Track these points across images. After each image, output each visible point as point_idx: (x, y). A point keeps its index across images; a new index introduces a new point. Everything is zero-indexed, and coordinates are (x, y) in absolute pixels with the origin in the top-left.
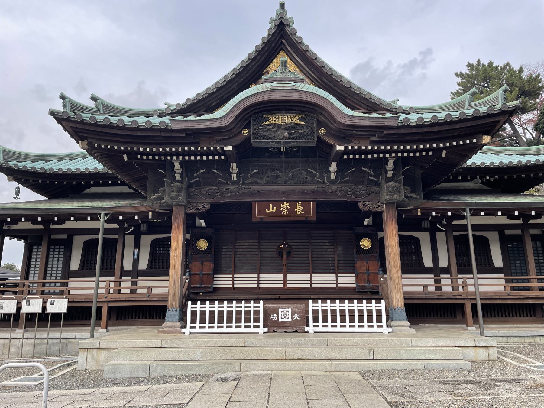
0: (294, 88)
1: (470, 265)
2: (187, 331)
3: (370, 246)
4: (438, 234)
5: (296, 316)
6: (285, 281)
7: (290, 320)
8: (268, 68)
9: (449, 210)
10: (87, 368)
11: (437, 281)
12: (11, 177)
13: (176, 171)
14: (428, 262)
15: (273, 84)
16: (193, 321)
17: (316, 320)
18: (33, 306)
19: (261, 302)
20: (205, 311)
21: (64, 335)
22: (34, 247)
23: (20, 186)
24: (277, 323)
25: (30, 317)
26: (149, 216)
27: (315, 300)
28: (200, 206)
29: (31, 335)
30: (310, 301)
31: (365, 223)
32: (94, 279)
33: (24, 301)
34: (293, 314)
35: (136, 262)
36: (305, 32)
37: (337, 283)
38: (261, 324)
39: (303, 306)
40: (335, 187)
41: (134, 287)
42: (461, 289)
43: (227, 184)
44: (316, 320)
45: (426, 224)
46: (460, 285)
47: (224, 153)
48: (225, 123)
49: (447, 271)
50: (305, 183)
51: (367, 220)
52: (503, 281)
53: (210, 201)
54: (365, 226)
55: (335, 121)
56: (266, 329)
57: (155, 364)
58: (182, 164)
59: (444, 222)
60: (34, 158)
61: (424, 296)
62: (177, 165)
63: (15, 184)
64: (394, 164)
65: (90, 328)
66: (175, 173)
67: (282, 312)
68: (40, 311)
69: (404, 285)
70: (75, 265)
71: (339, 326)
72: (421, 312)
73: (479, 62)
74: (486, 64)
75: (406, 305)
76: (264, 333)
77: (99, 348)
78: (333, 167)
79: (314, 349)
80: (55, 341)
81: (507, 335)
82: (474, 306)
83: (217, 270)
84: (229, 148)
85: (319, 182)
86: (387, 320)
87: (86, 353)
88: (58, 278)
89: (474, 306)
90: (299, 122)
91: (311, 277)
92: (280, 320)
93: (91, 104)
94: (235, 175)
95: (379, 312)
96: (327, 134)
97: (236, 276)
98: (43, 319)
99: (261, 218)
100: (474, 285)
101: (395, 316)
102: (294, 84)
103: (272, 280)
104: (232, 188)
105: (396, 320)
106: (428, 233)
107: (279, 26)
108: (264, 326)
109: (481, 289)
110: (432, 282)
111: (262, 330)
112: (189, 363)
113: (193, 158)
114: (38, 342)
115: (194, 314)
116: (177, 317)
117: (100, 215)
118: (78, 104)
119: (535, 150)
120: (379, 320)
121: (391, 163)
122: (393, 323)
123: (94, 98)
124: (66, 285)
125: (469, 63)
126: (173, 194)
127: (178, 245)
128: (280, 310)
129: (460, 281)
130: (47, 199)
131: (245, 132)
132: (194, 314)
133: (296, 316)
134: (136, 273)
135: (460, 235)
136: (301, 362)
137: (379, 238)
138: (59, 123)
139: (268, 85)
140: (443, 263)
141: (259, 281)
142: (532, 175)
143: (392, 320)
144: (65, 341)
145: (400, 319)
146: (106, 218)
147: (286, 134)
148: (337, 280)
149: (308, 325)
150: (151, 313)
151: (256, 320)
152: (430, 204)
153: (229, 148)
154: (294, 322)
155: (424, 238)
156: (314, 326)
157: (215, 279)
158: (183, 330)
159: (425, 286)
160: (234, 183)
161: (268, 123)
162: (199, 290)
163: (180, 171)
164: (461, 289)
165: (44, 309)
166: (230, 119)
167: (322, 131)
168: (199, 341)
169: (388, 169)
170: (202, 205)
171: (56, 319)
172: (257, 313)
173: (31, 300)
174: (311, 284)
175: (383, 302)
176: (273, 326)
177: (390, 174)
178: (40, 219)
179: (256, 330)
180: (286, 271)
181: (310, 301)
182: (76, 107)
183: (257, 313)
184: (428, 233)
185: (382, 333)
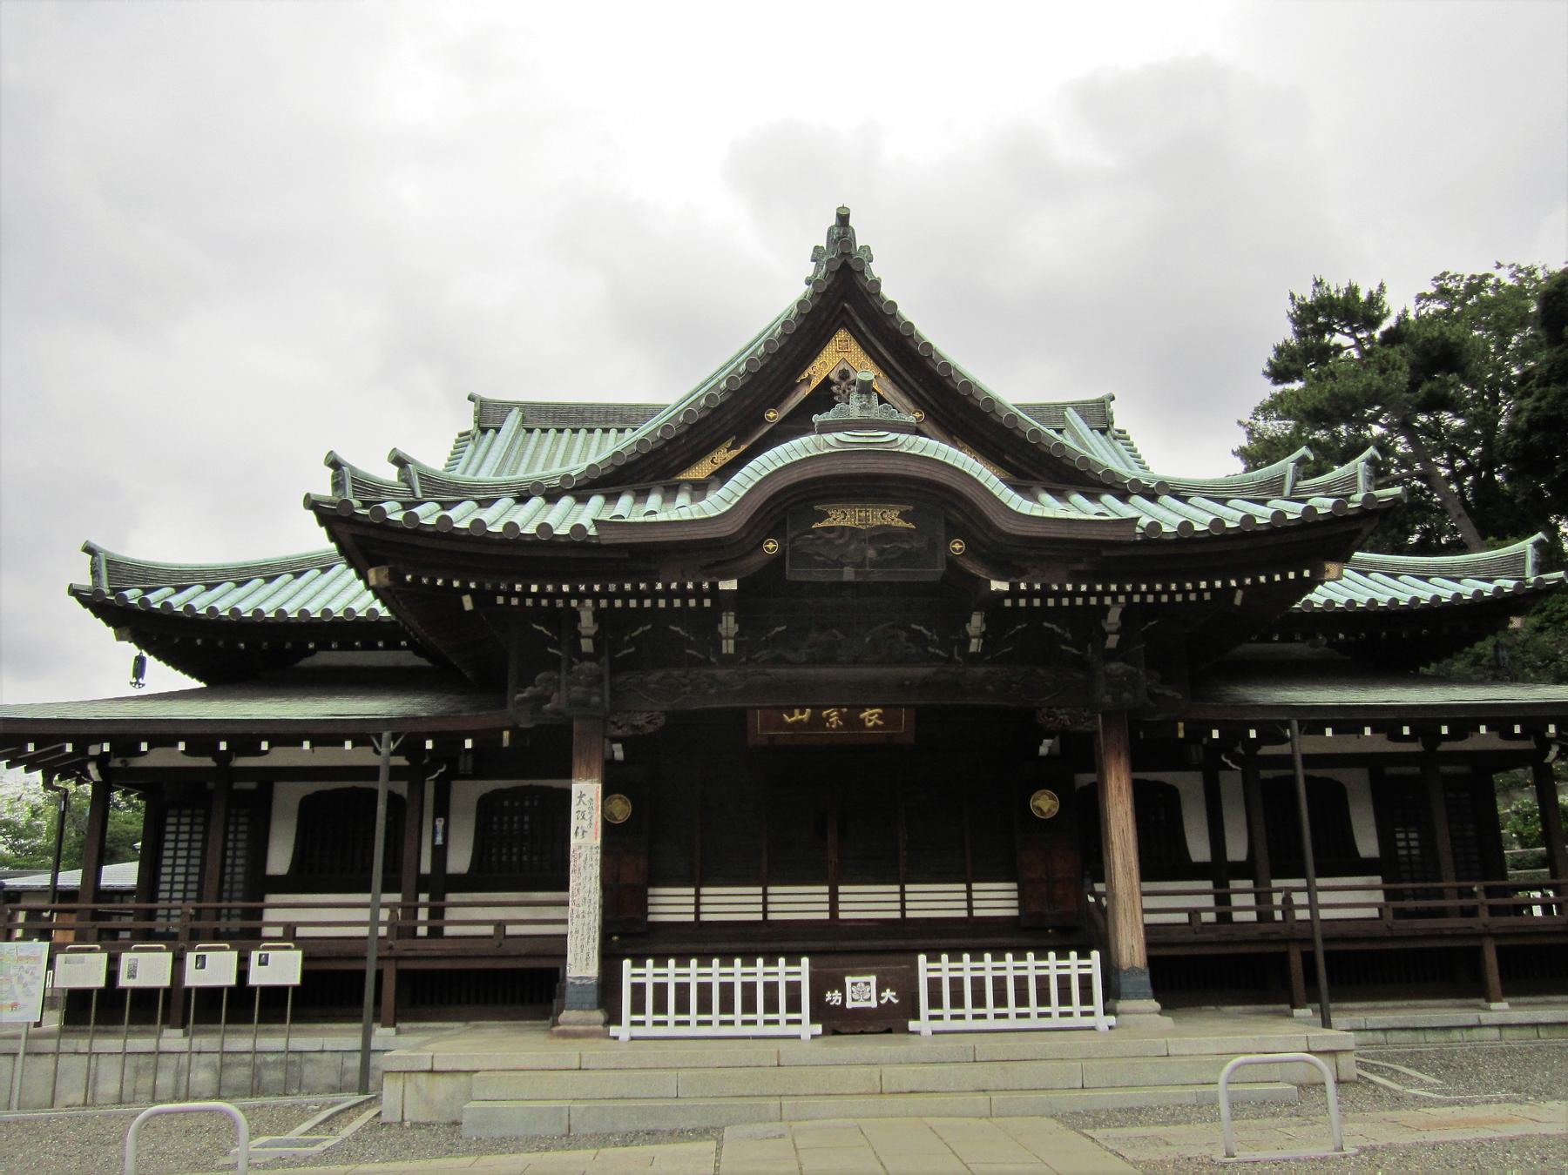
0: (889, 448)
1: (1300, 855)
2: (623, 1031)
3: (1055, 810)
4: (1222, 774)
7: (873, 1004)
8: (809, 371)
9: (1252, 725)
10: (406, 1117)
11: (1223, 899)
12: (126, 632)
13: (583, 632)
14: (1199, 850)
15: (841, 436)
16: (638, 1007)
17: (935, 1001)
18: (215, 968)
19: (805, 961)
20: (666, 985)
21: (299, 1043)
22: (171, 812)
23: (145, 654)
25: (209, 996)
26: (501, 739)
27: (933, 956)
28: (640, 720)
29: (206, 1042)
30: (922, 958)
31: (1043, 750)
33: (191, 957)
34: (880, 988)
36: (901, 284)
40: (980, 671)
41: (436, 923)
42: (1278, 915)
43: (707, 663)
44: (935, 1001)
45: (1196, 753)
46: (1278, 908)
47: (714, 591)
48: (728, 529)
49: (1240, 871)
50: (904, 660)
51: (1047, 742)
53: (666, 707)
54: (1044, 757)
55: (989, 525)
56: (818, 1029)
57: (577, 1105)
58: (598, 615)
59: (1240, 750)
60: (181, 579)
61: (1192, 937)
62: (587, 622)
63: (131, 650)
64: (1122, 616)
65: (360, 1025)
67: (854, 984)
68: (233, 982)
69: (1145, 911)
70: (279, 861)
71: (969, 1017)
75: (1152, 961)
76: (813, 1037)
77: (431, 1071)
78: (976, 623)
79: (945, 1067)
80: (270, 1058)
81: (1385, 1026)
82: (1309, 960)
84: (730, 585)
85: (937, 658)
86: (1106, 998)
87: (400, 1083)
89: (1309, 960)
90: (902, 524)
91: (902, 892)
92: (849, 1005)
93: (390, 474)
94: (731, 642)
95: (1086, 981)
96: (971, 550)
97: (704, 890)
98: (241, 1004)
99: (772, 738)
100: (1307, 889)
101: (1126, 987)
102: (892, 436)
103: (800, 903)
104: (721, 673)
105: (1128, 997)
106: (1199, 774)
108: (813, 1020)
110: (1209, 901)
111: (809, 1029)
112: (660, 1103)
113: (633, 603)
114: (228, 1058)
115: (638, 990)
118: (367, 477)
120: (1087, 998)
122: (1122, 1005)
123: (400, 461)
124: (257, 914)
126: (577, 692)
128: (848, 980)
129: (1277, 899)
130: (203, 685)
131: (771, 546)
132: (638, 990)
138: (321, 524)
139: (830, 438)
140: (1237, 850)
143: (1118, 997)
144: (296, 1058)
145: (1137, 996)
146: (392, 747)
147: (871, 553)
149: (917, 1017)
150: (520, 987)
153: (730, 585)
154: (884, 1010)
155: (1189, 784)
156: (932, 1018)
158: (613, 1030)
159: (1194, 913)
160: (728, 661)
161: (825, 524)
163: (592, 632)
164: (1278, 915)
168: (650, 1052)
169: (1107, 628)
170: (644, 715)
171: (272, 1005)
172: (794, 988)
173: (208, 954)
174: (903, 910)
175: (1095, 954)
176: (836, 1021)
177: (1112, 641)
179: (793, 1030)
180: (834, 877)
181: (922, 958)
182: (370, 489)
183: (794, 988)
184: (1199, 774)
185: (1093, 1028)
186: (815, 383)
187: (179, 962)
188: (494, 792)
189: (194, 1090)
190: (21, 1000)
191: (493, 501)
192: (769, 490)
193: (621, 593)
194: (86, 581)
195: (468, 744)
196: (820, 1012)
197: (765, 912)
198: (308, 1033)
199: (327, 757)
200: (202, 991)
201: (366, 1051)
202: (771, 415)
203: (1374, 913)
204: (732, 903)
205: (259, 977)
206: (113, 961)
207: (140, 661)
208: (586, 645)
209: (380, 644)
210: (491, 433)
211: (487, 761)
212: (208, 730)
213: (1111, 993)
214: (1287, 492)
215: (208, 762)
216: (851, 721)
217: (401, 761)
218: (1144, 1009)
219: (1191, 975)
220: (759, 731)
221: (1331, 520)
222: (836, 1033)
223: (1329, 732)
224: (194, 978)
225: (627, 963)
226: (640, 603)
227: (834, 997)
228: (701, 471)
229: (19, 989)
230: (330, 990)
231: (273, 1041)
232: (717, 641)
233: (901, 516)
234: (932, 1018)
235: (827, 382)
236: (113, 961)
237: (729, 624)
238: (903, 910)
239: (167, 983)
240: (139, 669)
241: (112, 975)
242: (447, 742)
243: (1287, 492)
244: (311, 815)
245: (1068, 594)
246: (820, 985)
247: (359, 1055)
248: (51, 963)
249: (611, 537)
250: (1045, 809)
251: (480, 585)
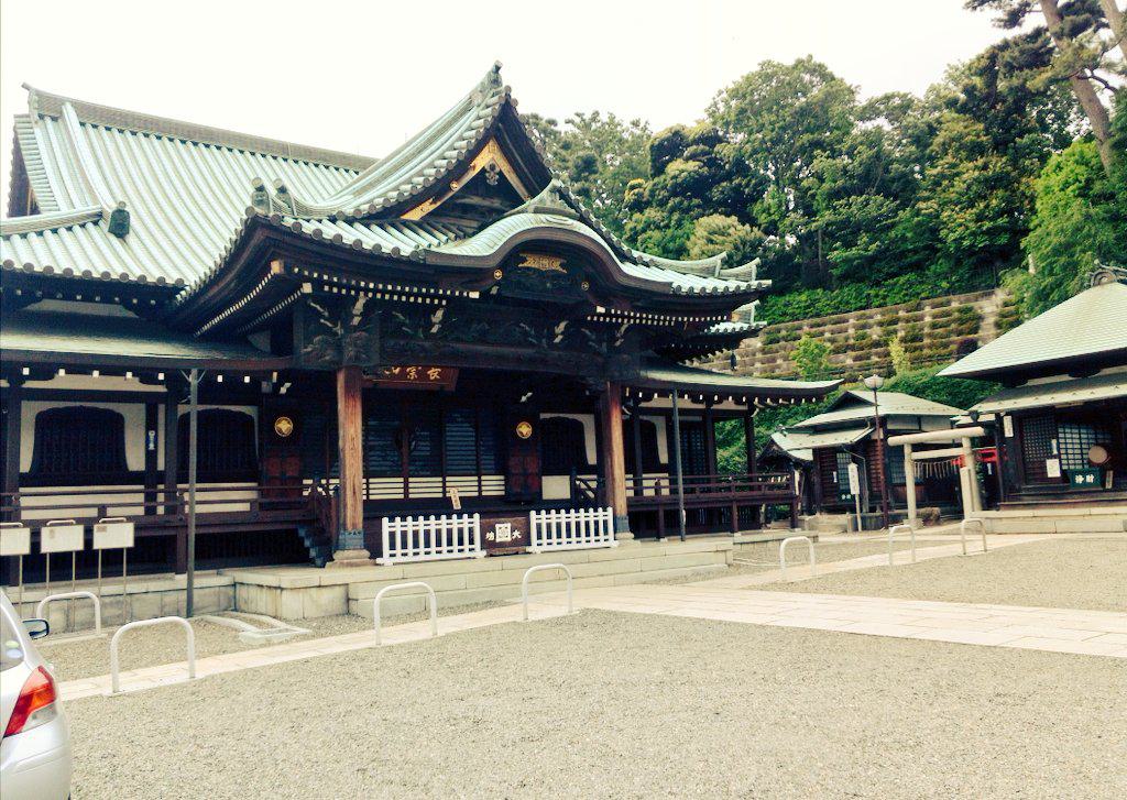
2: (385, 559)
6: (406, 488)
7: (509, 539)
15: (548, 217)
34: (513, 531)
35: (151, 457)
56: (485, 553)
75: (629, 514)
77: (320, 586)
86: (615, 532)
88: (652, 483)
98: (88, 563)
121: (359, 305)
127: (356, 431)
128: (497, 526)
133: (516, 534)
135: (67, 408)
137: (179, 414)
154: (515, 542)
157: (503, 488)
161: (525, 265)
169: (354, 312)
176: (492, 548)
177: (356, 320)
178: (161, 377)
186: (478, 170)
188: (53, 409)
189: (136, 611)
193: (340, 286)
196: (486, 544)
198: (111, 583)
200: (106, 552)
201: (190, 589)
202: (454, 185)
203: (245, 507)
209: (79, 297)
212: (14, 357)
214: (717, 274)
216: (422, 375)
219: (647, 522)
222: (491, 556)
226: (331, 289)
227: (490, 536)
231: (112, 586)
233: (561, 265)
234: (391, 555)
235: (483, 170)
243: (717, 274)
245: (388, 292)
247: (185, 592)
250: (525, 433)
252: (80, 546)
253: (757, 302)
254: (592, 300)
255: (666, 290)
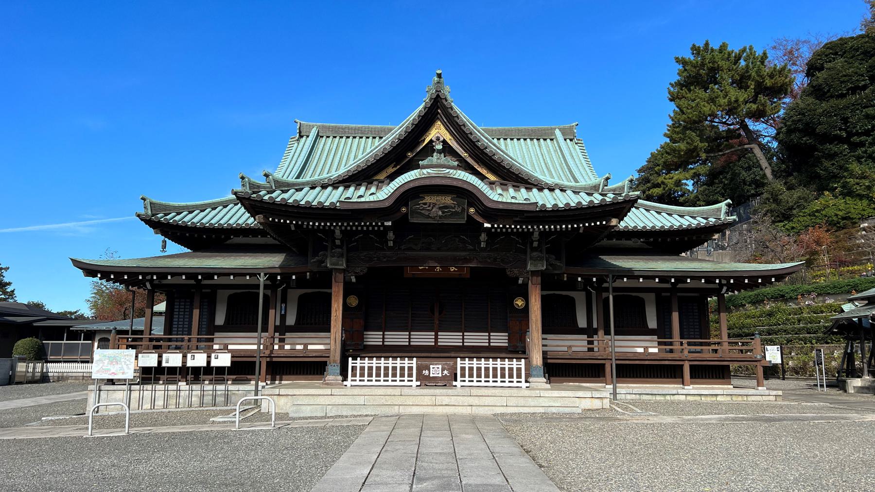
2: (348, 383)
5: (446, 372)
6: (436, 339)
7: (440, 375)
14: (582, 323)
15: (429, 170)
16: (354, 375)
17: (463, 375)
18: (198, 360)
24: (428, 378)
27: (463, 358)
32: (255, 334)
33: (189, 356)
34: (443, 370)
37: (489, 343)
38: (414, 378)
39: (452, 363)
40: (485, 254)
44: (463, 375)
48: (387, 204)
52: (656, 344)
56: (419, 383)
62: (338, 232)
63: (161, 238)
66: (335, 239)
68: (156, 365)
70: (220, 320)
72: (558, 370)
73: (707, 44)
74: (716, 47)
78: (483, 237)
83: (368, 328)
84: (390, 223)
92: (431, 375)
95: (519, 370)
97: (386, 333)
101: (534, 373)
102: (448, 170)
103: (423, 338)
107: (435, 99)
109: (617, 350)
111: (415, 383)
116: (339, 371)
117: (260, 274)
119: (693, 212)
120: (519, 376)
122: (530, 380)
125: (694, 45)
128: (431, 366)
133: (446, 372)
134: (283, 329)
136: (447, 407)
139: (425, 171)
141: (410, 338)
142: (686, 239)
148: (489, 339)
149: (456, 380)
150: (311, 368)
151: (410, 375)
152: (574, 270)
153: (390, 223)
154: (444, 377)
158: (345, 383)
160: (390, 248)
162: (353, 347)
165: (209, 362)
166: (391, 201)
167: (472, 210)
168: (356, 391)
174: (489, 343)
176: (425, 381)
179: (410, 383)
180: (437, 329)
181: (459, 359)
187: (185, 357)
190: (126, 371)
191: (301, 189)
192: (402, 190)
194: (142, 211)
195: (294, 277)
197: (410, 342)
199: (239, 281)
200: (193, 368)
204: (397, 338)
205: (214, 363)
206: (160, 356)
207: (164, 242)
208: (338, 242)
210: (304, 138)
211: (302, 282)
213: (528, 376)
215: (192, 282)
217: (269, 282)
218: (540, 381)
220: (409, 272)
221: (612, 204)
223: (625, 280)
224: (190, 363)
225: (350, 359)
227: (426, 372)
228: (382, 176)
229: (125, 367)
230: (242, 369)
232: (387, 241)
235: (431, 141)
236: (160, 356)
237: (391, 235)
238: (463, 342)
239: (180, 365)
240: (164, 247)
241: (160, 362)
242: (286, 277)
244: (232, 303)
246: (419, 369)
248: (137, 357)
249: (346, 207)
251: (297, 222)
252: (205, 365)
253: (729, 201)
254: (480, 220)
255: (532, 208)
